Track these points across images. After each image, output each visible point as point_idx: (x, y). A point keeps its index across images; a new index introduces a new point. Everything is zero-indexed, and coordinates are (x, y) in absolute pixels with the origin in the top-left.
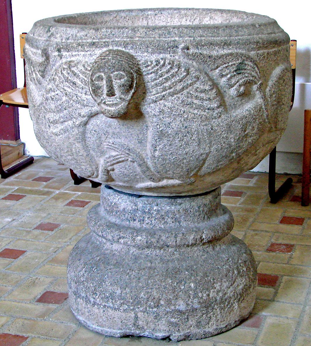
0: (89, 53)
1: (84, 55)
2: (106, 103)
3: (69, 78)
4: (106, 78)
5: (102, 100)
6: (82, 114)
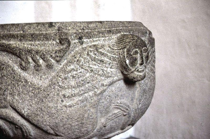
0: (107, 38)
1: (104, 40)
2: (139, 70)
3: (97, 57)
4: (140, 52)
5: (136, 68)
6: (105, 84)
